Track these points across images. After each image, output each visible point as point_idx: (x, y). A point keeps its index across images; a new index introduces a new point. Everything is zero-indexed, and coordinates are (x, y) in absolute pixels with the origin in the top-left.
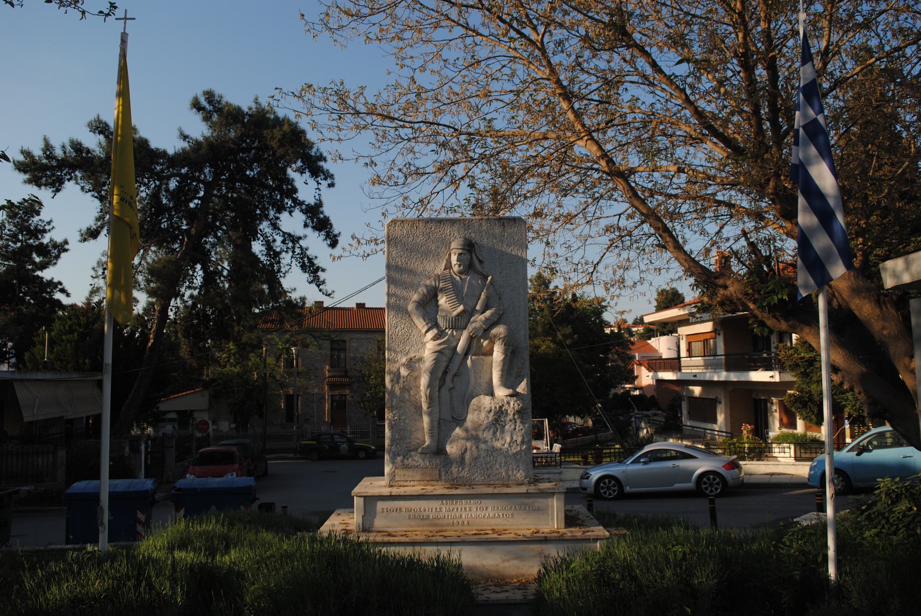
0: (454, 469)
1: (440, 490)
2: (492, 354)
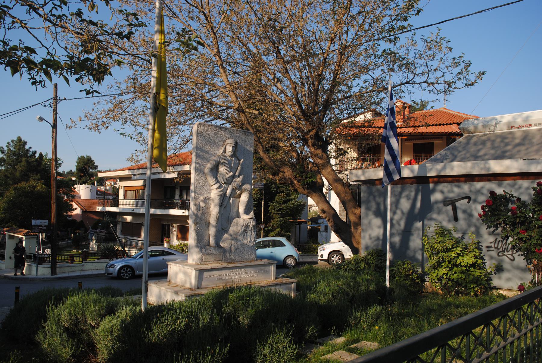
0: (228, 255)
1: (225, 265)
2: (240, 198)
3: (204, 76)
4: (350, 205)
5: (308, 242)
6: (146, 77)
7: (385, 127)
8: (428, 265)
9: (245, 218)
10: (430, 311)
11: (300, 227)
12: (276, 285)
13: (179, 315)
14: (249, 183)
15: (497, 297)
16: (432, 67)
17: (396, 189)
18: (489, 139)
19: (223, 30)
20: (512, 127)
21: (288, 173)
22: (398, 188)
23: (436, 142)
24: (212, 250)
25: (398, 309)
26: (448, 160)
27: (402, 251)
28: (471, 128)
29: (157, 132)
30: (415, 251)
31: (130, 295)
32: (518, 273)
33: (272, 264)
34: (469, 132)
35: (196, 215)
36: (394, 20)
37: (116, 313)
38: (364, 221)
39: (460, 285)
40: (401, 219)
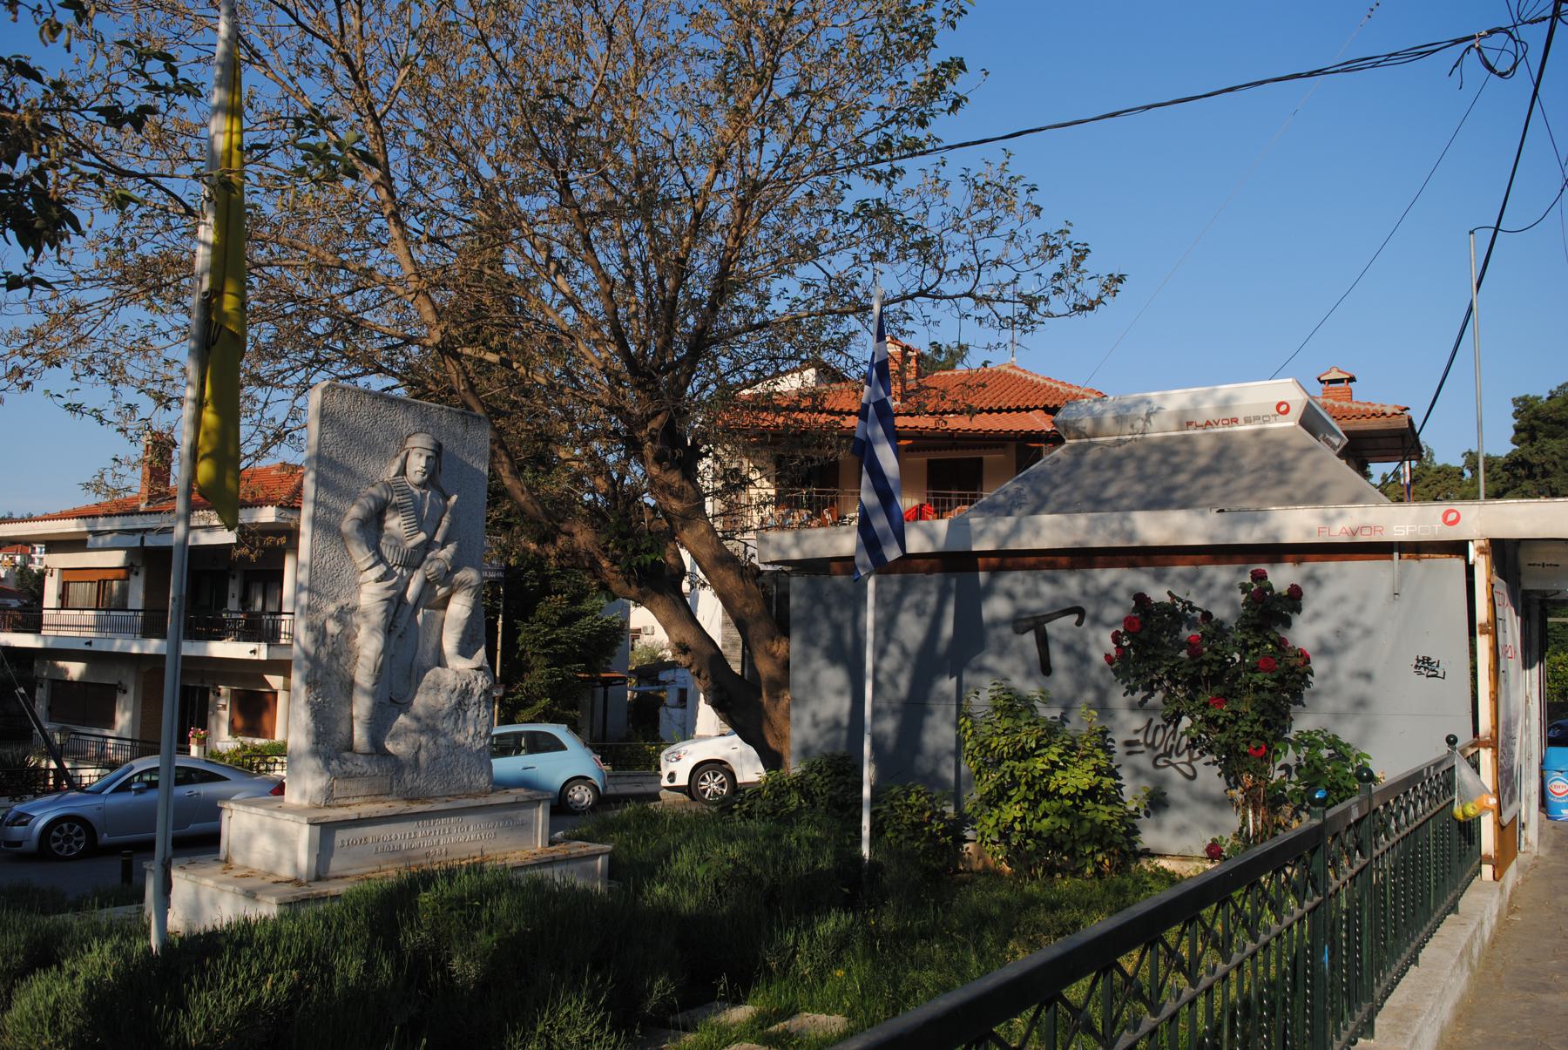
0: (408, 777)
1: (400, 807)
2: (445, 608)
3: (337, 243)
4: (759, 630)
5: (628, 738)
6: (158, 238)
7: (862, 414)
8: (973, 797)
9: (460, 668)
10: (981, 921)
11: (606, 694)
12: (552, 862)
13: (271, 958)
14: (473, 566)
15: (1154, 876)
16: (988, 256)
17: (886, 587)
18: (1130, 454)
19: (400, 113)
20: (1189, 424)
21: (583, 537)
22: (894, 582)
23: (989, 457)
24: (362, 764)
25: (897, 919)
26: (1025, 509)
27: (901, 759)
28: (1086, 423)
29: (210, 408)
30: (937, 759)
31: (101, 906)
32: (1204, 811)
33: (539, 802)
34: (1080, 434)
35: (314, 660)
36: (890, 122)
37: (66, 963)
38: (799, 676)
39: (1057, 847)
40: (900, 670)
